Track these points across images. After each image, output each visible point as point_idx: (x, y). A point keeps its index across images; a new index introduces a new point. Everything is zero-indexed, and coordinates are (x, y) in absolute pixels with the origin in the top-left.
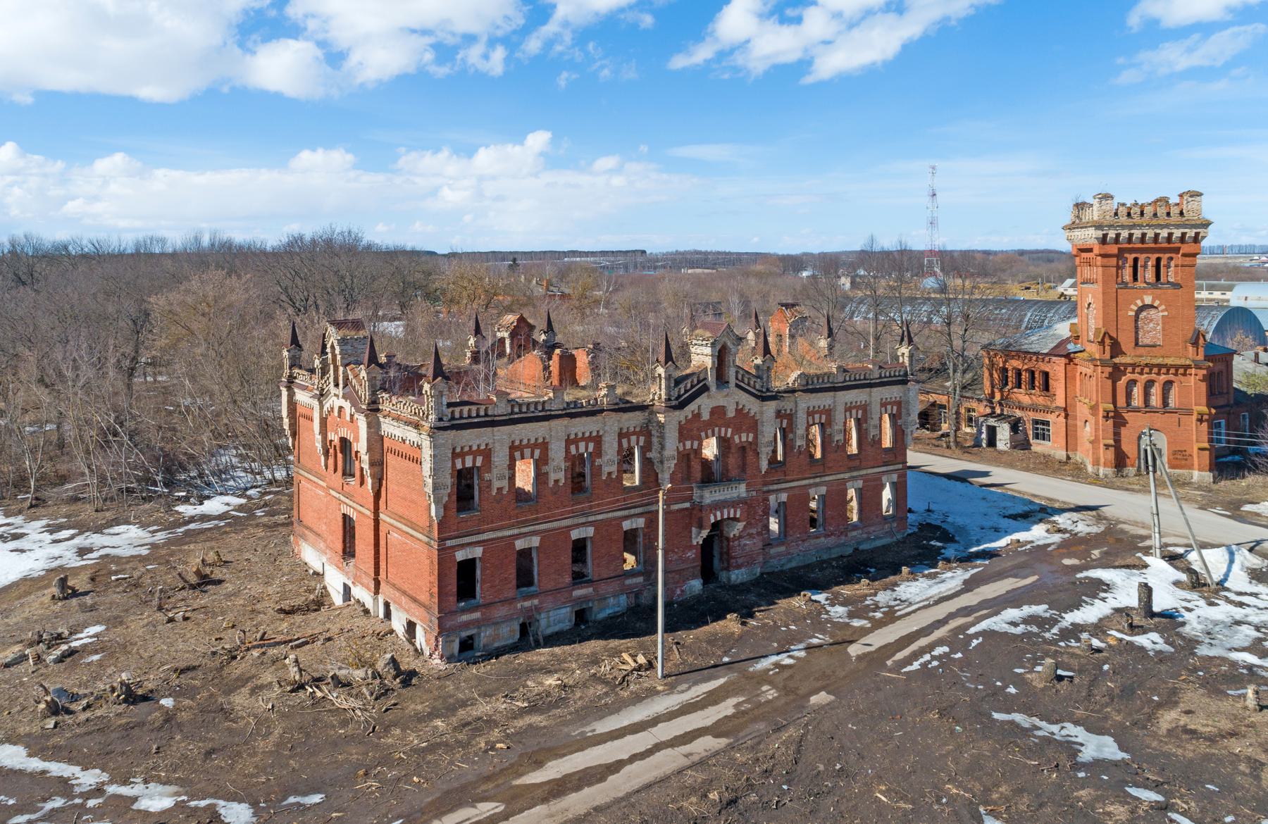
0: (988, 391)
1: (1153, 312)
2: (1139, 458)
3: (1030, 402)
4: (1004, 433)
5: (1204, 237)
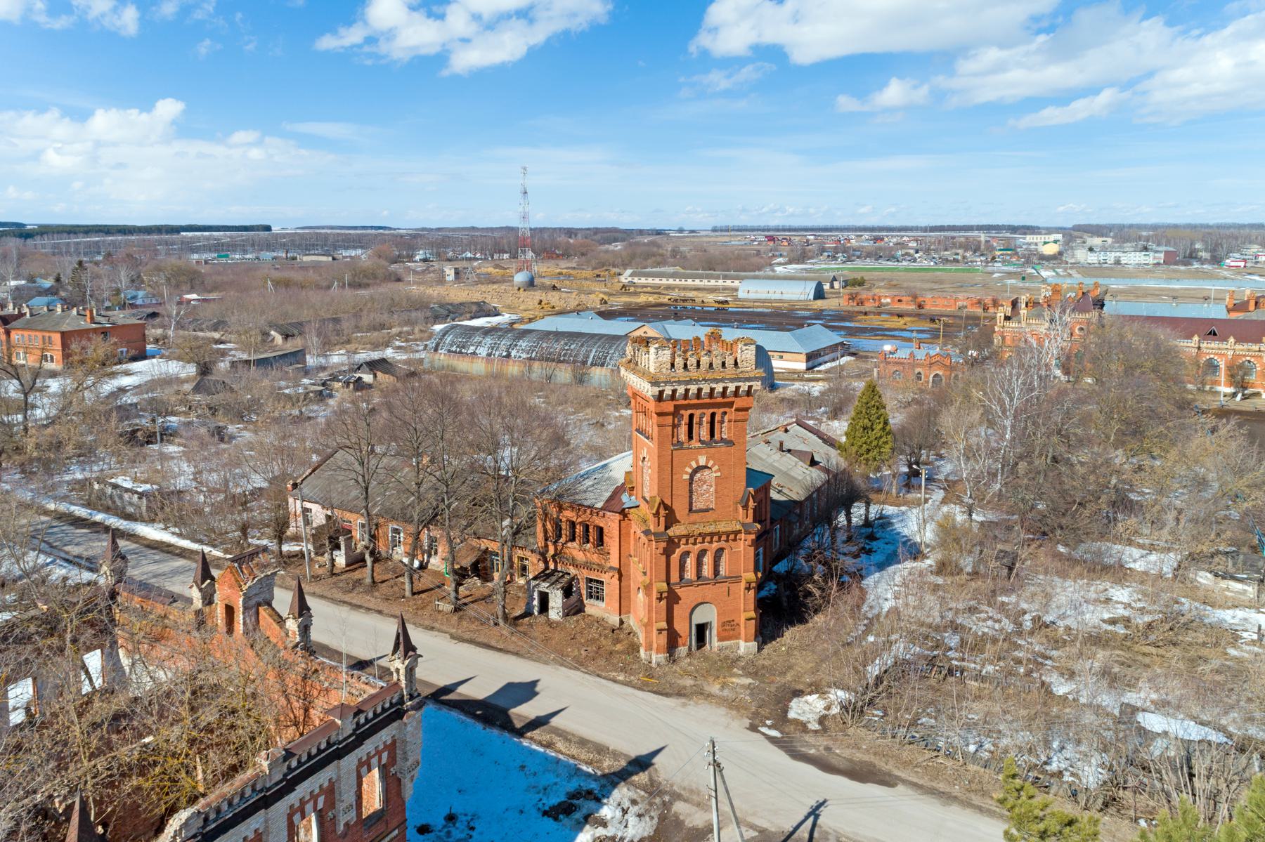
0: (541, 543)
1: (706, 472)
2: (690, 635)
3: (584, 559)
4: (556, 600)
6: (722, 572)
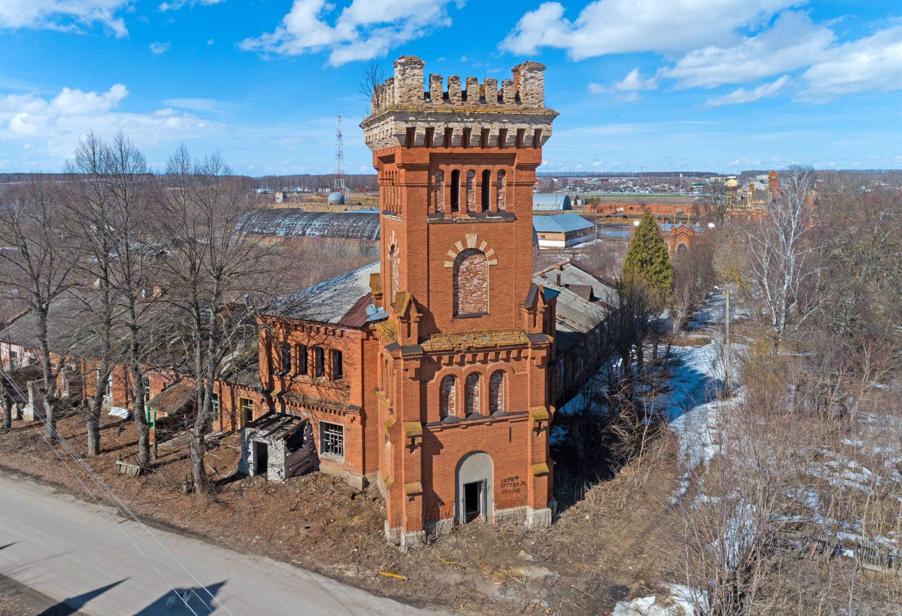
0: (265, 379)
1: (477, 259)
3: (318, 397)
4: (277, 454)
5: (546, 138)
6: (501, 407)
